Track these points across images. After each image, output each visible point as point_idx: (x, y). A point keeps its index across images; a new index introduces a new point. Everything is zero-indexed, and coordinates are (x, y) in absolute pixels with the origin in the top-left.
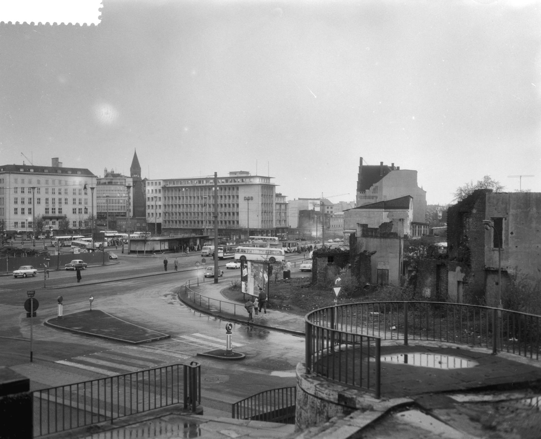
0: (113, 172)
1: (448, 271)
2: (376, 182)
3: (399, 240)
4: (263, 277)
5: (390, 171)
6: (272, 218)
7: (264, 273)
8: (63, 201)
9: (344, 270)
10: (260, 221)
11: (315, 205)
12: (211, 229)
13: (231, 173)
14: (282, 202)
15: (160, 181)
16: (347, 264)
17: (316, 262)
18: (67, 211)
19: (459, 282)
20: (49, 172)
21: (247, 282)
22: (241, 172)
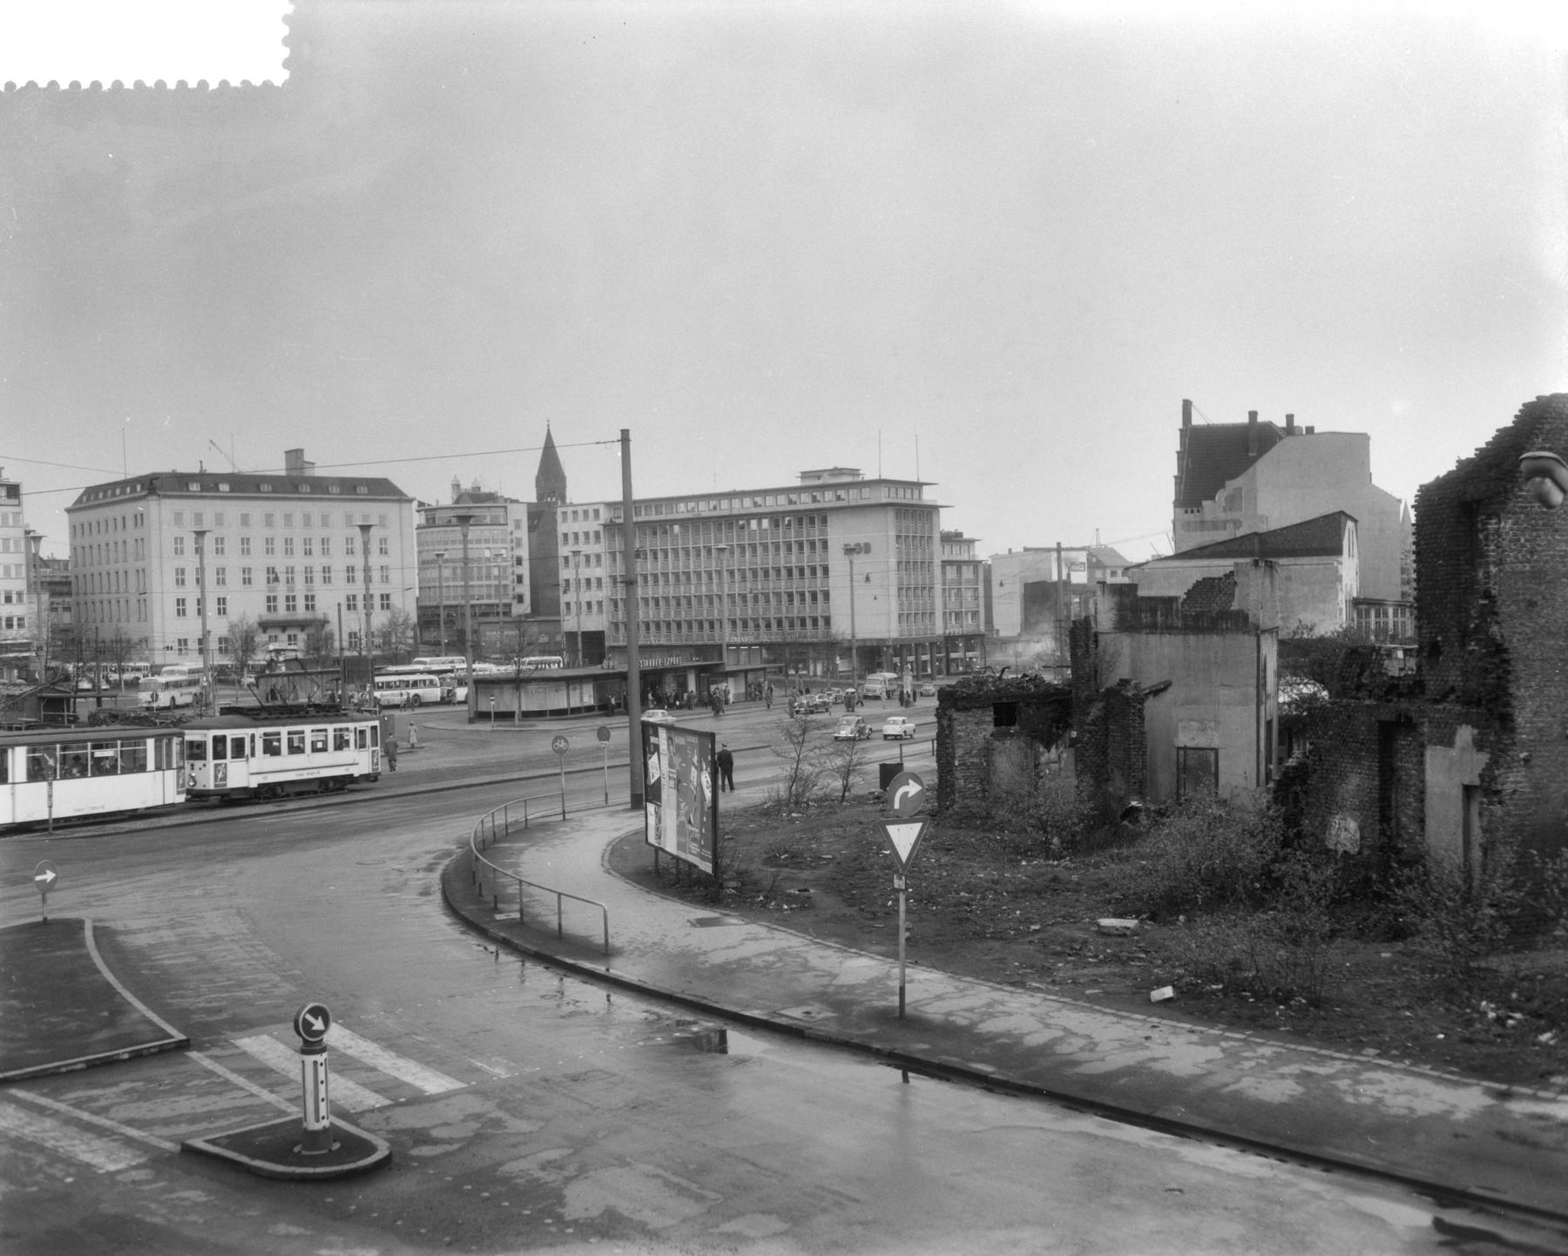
0: (479, 488)
1: (1423, 746)
2: (1233, 477)
3: (1253, 640)
4: (700, 784)
5: (1281, 438)
6: (933, 604)
7: (701, 770)
8: (318, 577)
9: (1053, 753)
10: (895, 617)
12: (750, 645)
13: (805, 475)
14: (965, 557)
15: (596, 507)
16: (1064, 731)
18: (328, 602)
19: (1468, 790)
20: (273, 492)
21: (660, 806)
22: (837, 472)
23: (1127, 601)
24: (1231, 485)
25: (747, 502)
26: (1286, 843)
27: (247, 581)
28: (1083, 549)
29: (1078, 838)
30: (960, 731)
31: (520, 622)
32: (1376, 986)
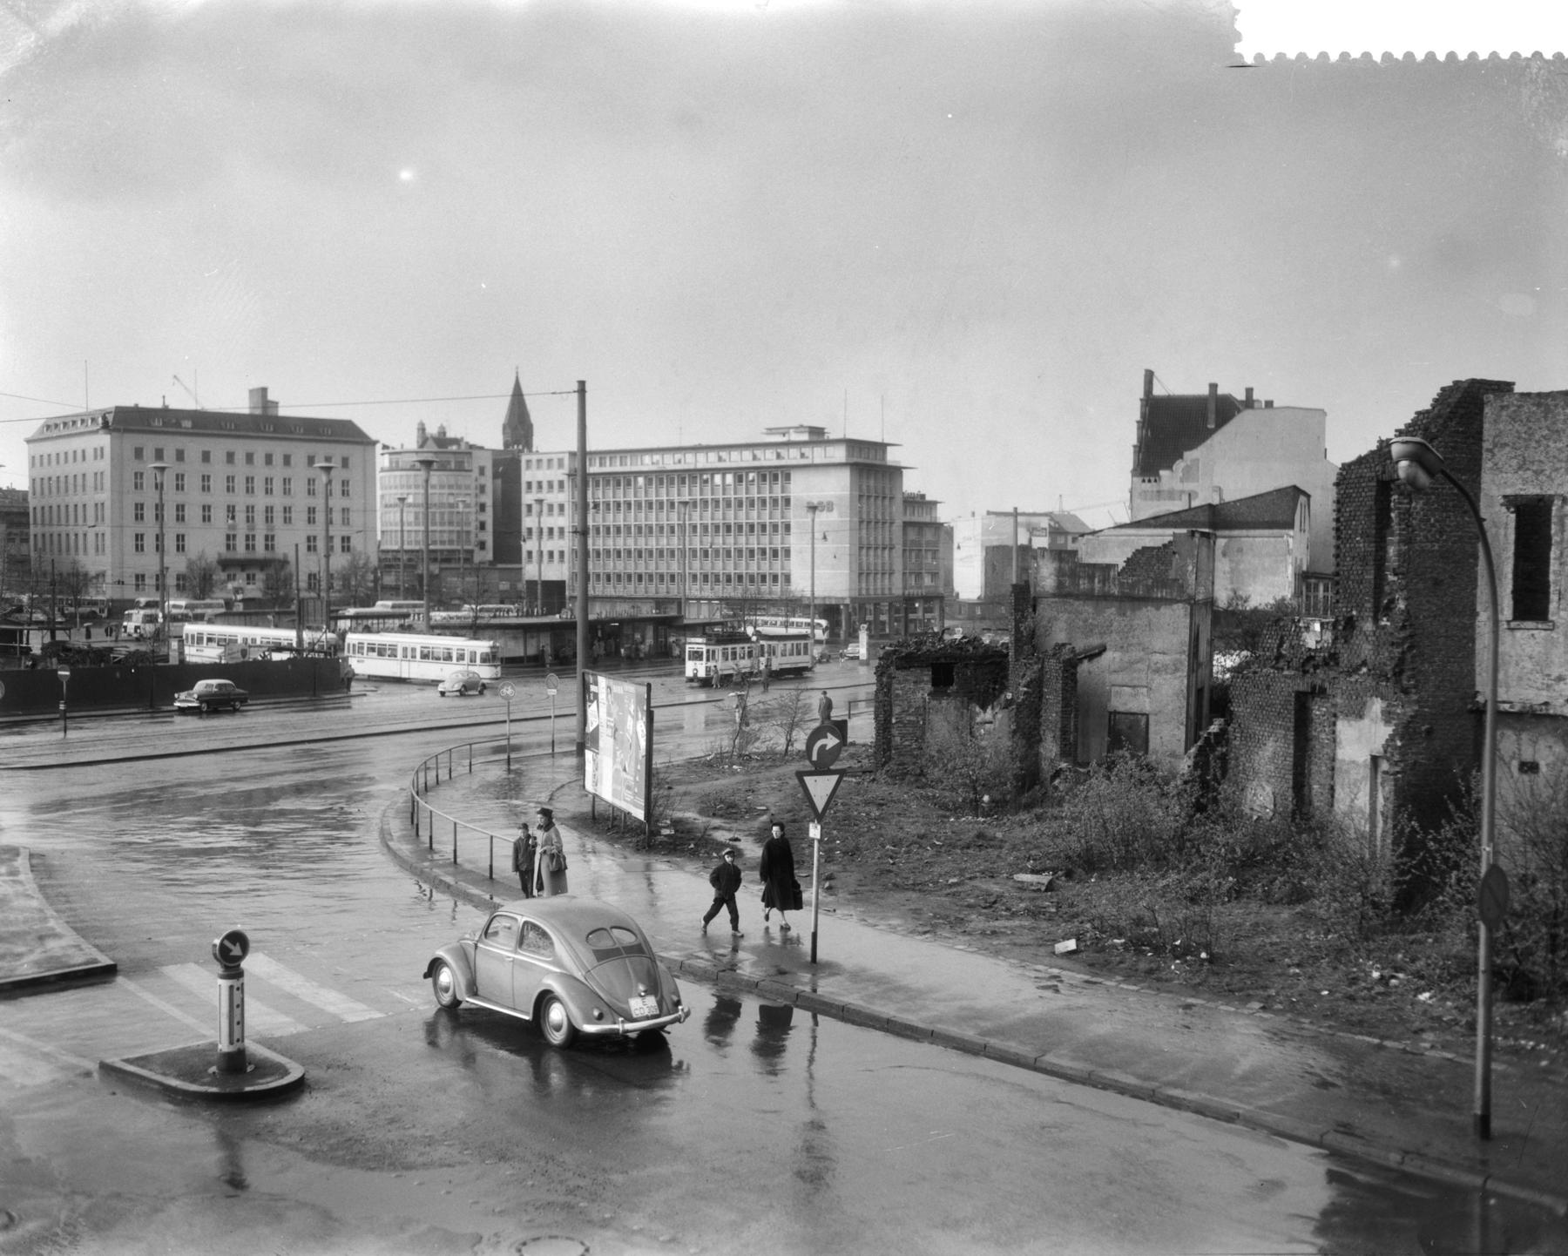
0: (444, 433)
2: (1191, 447)
5: (1239, 411)
8: (278, 516)
9: (988, 715)
11: (1032, 530)
12: (710, 600)
14: (927, 519)
15: (561, 456)
17: (889, 686)
18: (288, 541)
23: (1066, 567)
24: (1189, 455)
25: (713, 456)
26: (1200, 807)
27: (206, 519)
28: (1045, 515)
29: (1008, 797)
30: (898, 689)
31: (478, 570)
32: (1272, 944)
